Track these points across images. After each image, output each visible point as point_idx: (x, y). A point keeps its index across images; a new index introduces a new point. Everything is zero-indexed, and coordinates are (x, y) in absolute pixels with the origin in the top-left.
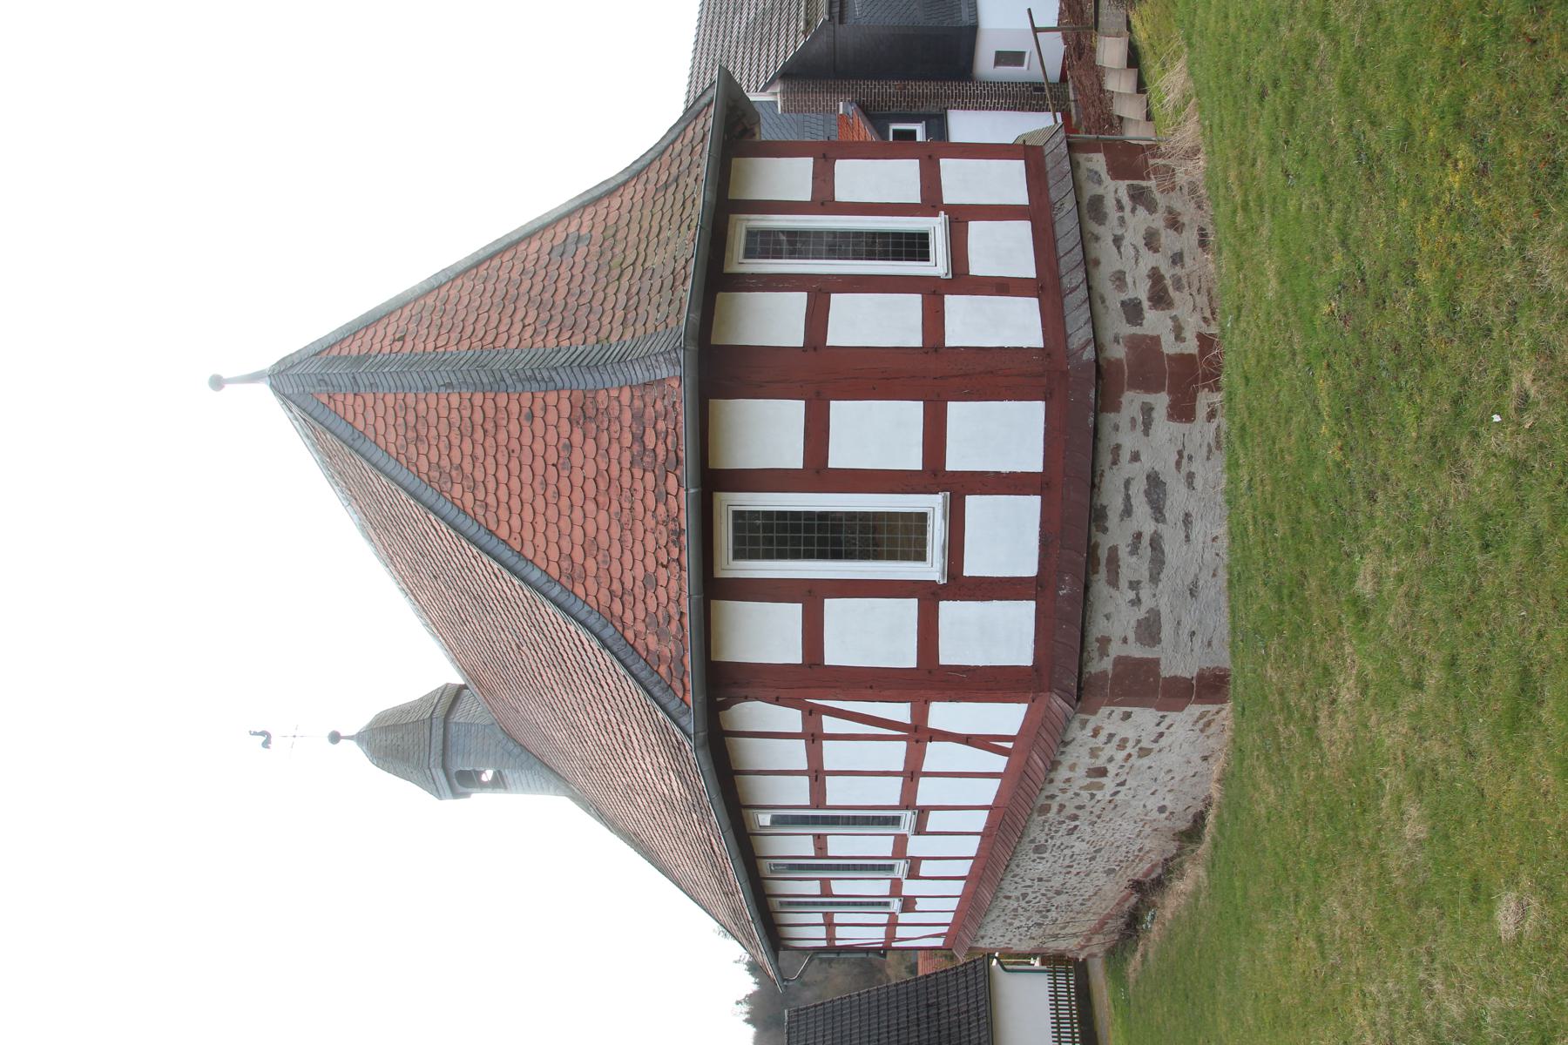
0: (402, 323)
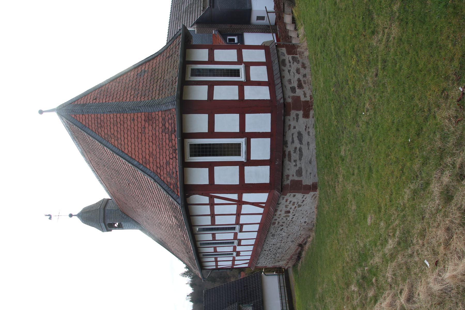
0: (95, 95)
